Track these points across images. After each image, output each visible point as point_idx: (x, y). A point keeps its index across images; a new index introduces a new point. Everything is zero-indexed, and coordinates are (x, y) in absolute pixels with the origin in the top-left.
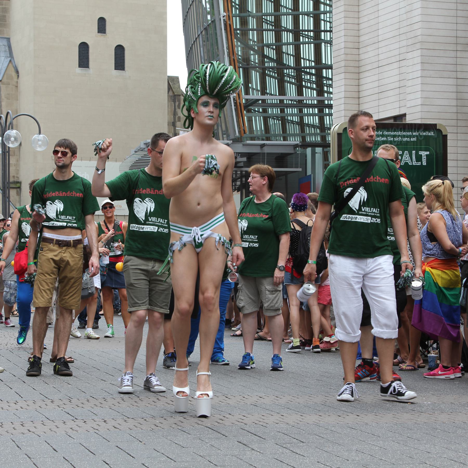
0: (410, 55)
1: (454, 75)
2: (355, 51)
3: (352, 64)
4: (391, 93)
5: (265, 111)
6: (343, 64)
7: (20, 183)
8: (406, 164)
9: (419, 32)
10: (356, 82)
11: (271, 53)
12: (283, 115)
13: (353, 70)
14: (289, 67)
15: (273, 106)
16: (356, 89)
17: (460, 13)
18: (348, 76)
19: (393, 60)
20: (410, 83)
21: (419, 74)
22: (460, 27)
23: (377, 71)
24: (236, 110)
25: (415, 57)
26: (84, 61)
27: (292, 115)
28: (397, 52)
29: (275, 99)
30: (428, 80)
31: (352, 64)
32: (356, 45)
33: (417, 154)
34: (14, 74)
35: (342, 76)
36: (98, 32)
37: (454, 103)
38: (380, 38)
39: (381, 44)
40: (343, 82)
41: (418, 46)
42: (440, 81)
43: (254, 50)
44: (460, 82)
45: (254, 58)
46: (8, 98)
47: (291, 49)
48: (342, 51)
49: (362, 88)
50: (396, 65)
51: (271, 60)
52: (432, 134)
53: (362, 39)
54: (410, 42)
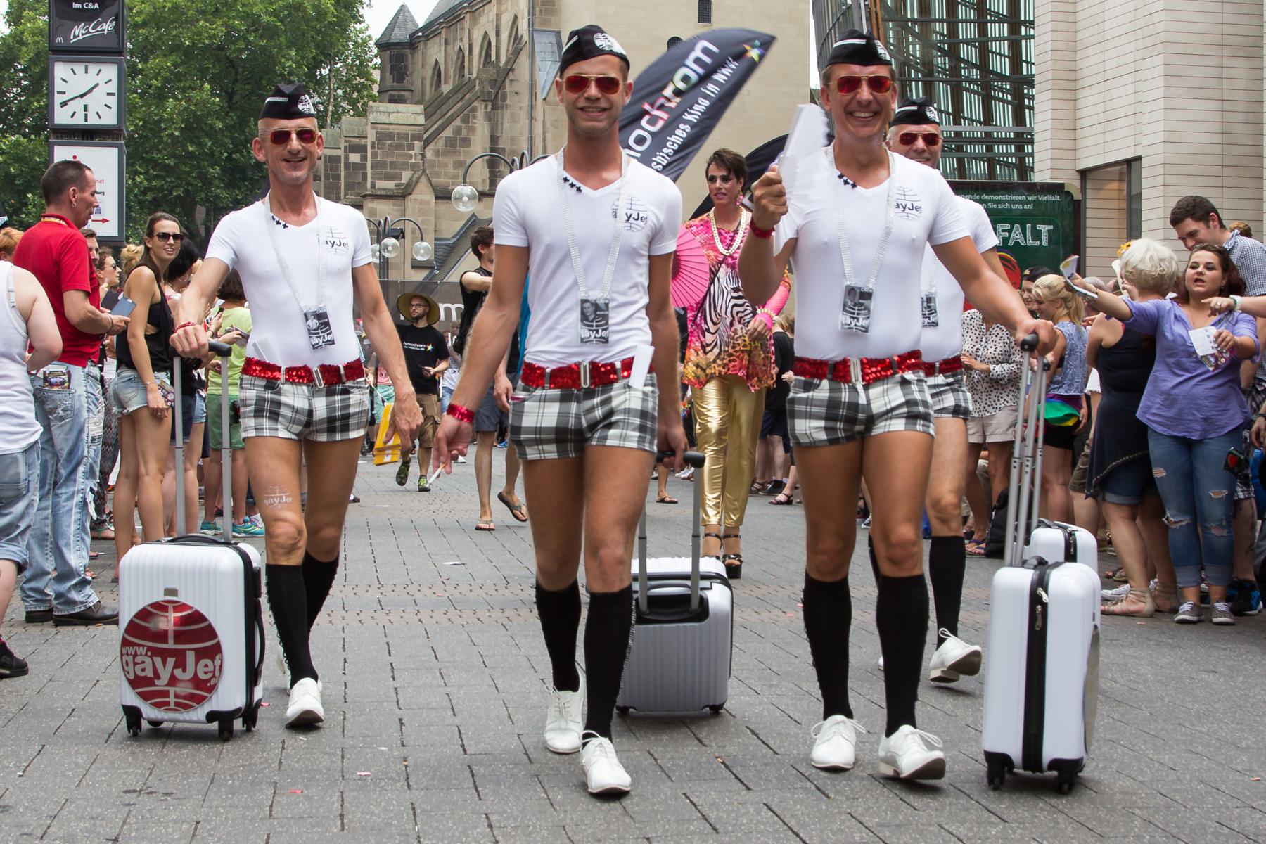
0: (1147, 64)
1: (1218, 94)
2: (1069, 56)
3: (1065, 76)
4: (1122, 122)
5: (959, 149)
6: (1049, 75)
8: (1017, 244)
9: (1161, 27)
10: (1070, 105)
12: (989, 155)
13: (1065, 85)
14: (1001, 77)
15: (973, 141)
16: (1070, 115)
18: (1059, 94)
20: (1147, 107)
22: (1228, 18)
23: (1102, 87)
25: (1155, 67)
27: (1008, 155)
28: (1131, 58)
29: (978, 130)
30: (1176, 103)
31: (1065, 76)
32: (1071, 46)
33: (1034, 229)
35: (1049, 94)
36: (699, 21)
37: (1217, 139)
38: (1107, 35)
39: (1108, 45)
40: (1049, 105)
41: (1160, 48)
44: (1227, 106)
45: (942, 62)
46: (556, 128)
47: (1005, 48)
48: (1049, 56)
49: (1079, 114)
52: (1056, 198)
53: (1079, 36)
54: (1149, 42)
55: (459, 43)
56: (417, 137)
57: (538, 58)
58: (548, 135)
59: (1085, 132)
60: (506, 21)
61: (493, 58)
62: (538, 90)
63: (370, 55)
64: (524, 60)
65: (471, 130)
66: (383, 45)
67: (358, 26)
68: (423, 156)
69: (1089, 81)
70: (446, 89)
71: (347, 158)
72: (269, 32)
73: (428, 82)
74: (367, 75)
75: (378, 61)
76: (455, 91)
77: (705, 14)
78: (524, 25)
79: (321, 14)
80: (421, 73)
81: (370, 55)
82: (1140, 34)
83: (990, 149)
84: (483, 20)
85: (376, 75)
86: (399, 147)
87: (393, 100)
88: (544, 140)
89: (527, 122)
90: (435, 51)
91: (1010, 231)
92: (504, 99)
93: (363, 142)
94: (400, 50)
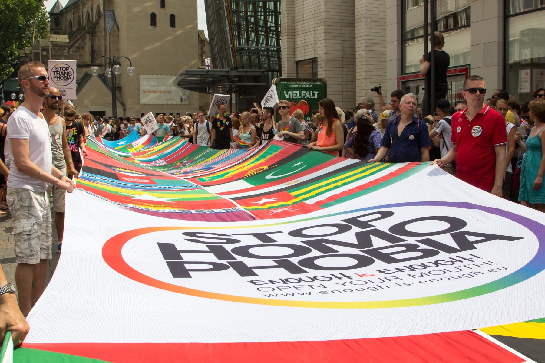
0: (319, 28)
2: (292, 25)
4: (310, 47)
5: (258, 53)
7: (121, 87)
11: (252, 20)
14: (261, 27)
17: (344, 8)
19: (311, 30)
20: (319, 42)
21: (323, 38)
22: (344, 14)
24: (232, 53)
25: (322, 29)
26: (153, 22)
28: (313, 26)
30: (328, 41)
33: (313, 93)
34: (116, 30)
37: (341, 52)
42: (334, 41)
43: (243, 18)
45: (243, 22)
47: (262, 18)
49: (296, 43)
50: (312, 33)
51: (252, 23)
52: (320, 83)
54: (319, 21)
55: (78, 14)
56: (66, 46)
57: (107, 19)
58: (111, 45)
59: (298, 49)
60: (95, 6)
61: (91, 19)
62: (107, 30)
63: (46, 17)
64: (102, 21)
65: (85, 44)
66: (51, 14)
67: (43, 8)
68: (69, 52)
69: (299, 33)
70: (74, 29)
71: (42, 53)
72: (13, 10)
73: (67, 27)
74: (46, 24)
75: (50, 19)
76: (78, 30)
77: (163, 5)
78: (102, 8)
79: (30, 4)
80: (65, 24)
81: (46, 17)
82: (316, 19)
83: (268, 53)
84: (87, 6)
85: (49, 24)
86: (60, 50)
87: (55, 33)
88: (110, 47)
89: (103, 41)
90: (70, 16)
91: (305, 94)
92: (96, 33)
93: (47, 48)
94: (57, 16)
